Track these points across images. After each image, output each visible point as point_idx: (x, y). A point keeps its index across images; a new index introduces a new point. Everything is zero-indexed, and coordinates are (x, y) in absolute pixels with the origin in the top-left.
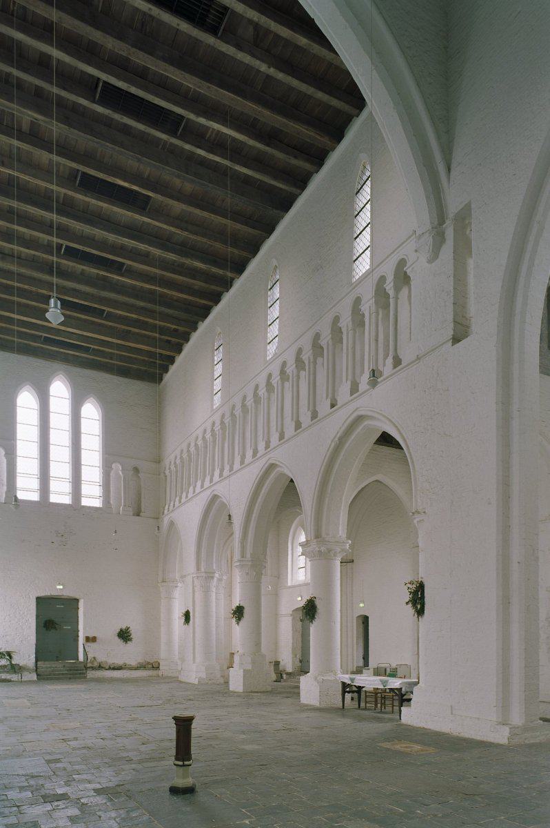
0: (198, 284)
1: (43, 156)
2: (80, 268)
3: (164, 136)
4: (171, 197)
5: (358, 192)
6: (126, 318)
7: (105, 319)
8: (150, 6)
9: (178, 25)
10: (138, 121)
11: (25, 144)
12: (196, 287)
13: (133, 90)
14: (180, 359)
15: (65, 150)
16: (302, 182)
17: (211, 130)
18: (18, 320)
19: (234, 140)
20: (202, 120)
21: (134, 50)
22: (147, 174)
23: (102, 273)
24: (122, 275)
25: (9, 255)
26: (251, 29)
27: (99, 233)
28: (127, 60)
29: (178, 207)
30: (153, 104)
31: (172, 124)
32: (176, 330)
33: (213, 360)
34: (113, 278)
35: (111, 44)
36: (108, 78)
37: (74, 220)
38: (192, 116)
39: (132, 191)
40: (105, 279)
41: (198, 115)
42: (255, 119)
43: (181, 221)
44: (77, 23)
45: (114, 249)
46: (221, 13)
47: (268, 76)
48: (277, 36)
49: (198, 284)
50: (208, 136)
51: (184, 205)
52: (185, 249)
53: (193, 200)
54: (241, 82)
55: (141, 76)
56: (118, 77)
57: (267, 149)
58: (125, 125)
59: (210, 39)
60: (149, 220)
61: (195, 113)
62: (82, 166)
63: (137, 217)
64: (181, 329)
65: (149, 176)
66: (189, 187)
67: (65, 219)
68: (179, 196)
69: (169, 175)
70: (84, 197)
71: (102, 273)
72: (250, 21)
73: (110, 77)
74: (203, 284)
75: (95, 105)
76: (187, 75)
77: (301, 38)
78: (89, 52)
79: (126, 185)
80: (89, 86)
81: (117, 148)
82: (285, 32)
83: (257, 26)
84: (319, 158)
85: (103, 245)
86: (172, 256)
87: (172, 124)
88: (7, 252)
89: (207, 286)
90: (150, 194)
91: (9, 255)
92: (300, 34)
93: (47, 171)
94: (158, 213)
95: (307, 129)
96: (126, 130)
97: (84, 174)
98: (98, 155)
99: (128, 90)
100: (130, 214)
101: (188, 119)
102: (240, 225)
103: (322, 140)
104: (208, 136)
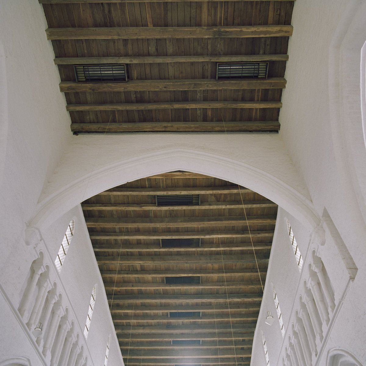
0: (243, 310)
1: (149, 277)
2: (180, 321)
3: (194, 249)
4: (209, 273)
5: (290, 233)
6: (225, 341)
7: (202, 345)
8: (169, 207)
9: (182, 208)
10: (181, 248)
11: (139, 275)
12: (243, 312)
13: (174, 237)
14: (253, 356)
15: (156, 271)
16: (269, 242)
17: (215, 239)
18: (245, 358)
19: (227, 238)
20: (207, 237)
21: (168, 224)
22: (195, 267)
23: (192, 320)
24: (201, 318)
25: (147, 326)
26: (213, 197)
27: (184, 301)
28: (170, 228)
29: (215, 276)
30: (184, 239)
31: (204, 243)
32: (244, 340)
33: (264, 351)
34: (199, 321)
35: (158, 225)
36: (162, 237)
37: (151, 299)
38: (202, 237)
39: (190, 277)
40: (194, 323)
41: (205, 236)
42: (233, 227)
43: (220, 282)
44: (144, 224)
45: (197, 306)
46: (198, 197)
47: (229, 209)
48: (225, 195)
49: (243, 310)
50: (215, 242)
51: (216, 274)
52: (141, 294)
53: (220, 270)
54: (219, 216)
55: (177, 231)
56: (167, 236)
57: (243, 236)
58: (178, 251)
59: (197, 207)
60: (203, 287)
61: (203, 235)
62: (164, 275)
63: (196, 287)
64: (246, 338)
65: (196, 268)
66: (216, 266)
67: (164, 300)
68: (213, 271)
69: (203, 263)
70: (170, 287)
71: (192, 320)
72: (211, 195)
73: (163, 237)
74: (245, 310)
75: (161, 249)
76: (193, 223)
77: (234, 190)
78: (155, 232)
79: (186, 275)
80: (156, 244)
81: (175, 262)
82: (226, 192)
83: (215, 195)
84: (272, 229)
85: (187, 306)
86: (221, 300)
87: (204, 243)
88: (145, 325)
89: (247, 309)
90: (198, 275)
91: (147, 326)
92: (233, 189)
93: (152, 282)
94: (207, 281)
95: (257, 221)
96: (178, 254)
97: (166, 277)
98: (171, 268)
99: (172, 238)
100: (192, 287)
101: (201, 239)
102: (240, 273)
103: (267, 222)
104: (215, 242)
